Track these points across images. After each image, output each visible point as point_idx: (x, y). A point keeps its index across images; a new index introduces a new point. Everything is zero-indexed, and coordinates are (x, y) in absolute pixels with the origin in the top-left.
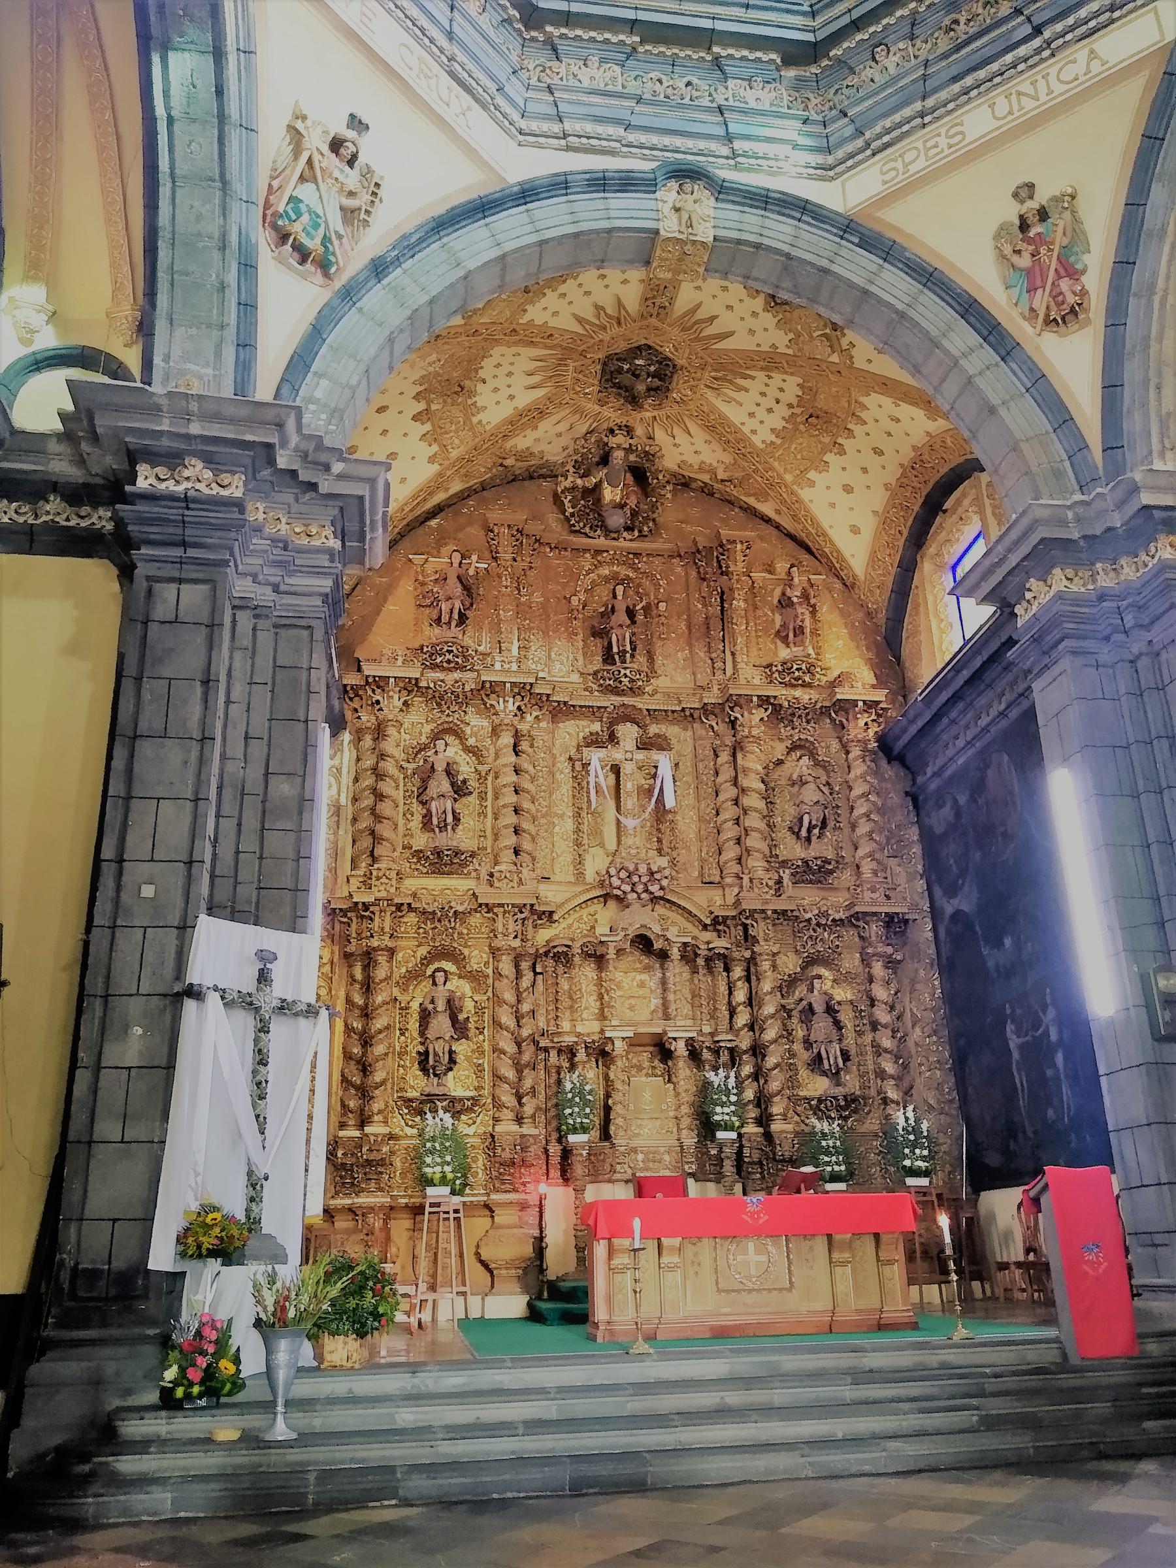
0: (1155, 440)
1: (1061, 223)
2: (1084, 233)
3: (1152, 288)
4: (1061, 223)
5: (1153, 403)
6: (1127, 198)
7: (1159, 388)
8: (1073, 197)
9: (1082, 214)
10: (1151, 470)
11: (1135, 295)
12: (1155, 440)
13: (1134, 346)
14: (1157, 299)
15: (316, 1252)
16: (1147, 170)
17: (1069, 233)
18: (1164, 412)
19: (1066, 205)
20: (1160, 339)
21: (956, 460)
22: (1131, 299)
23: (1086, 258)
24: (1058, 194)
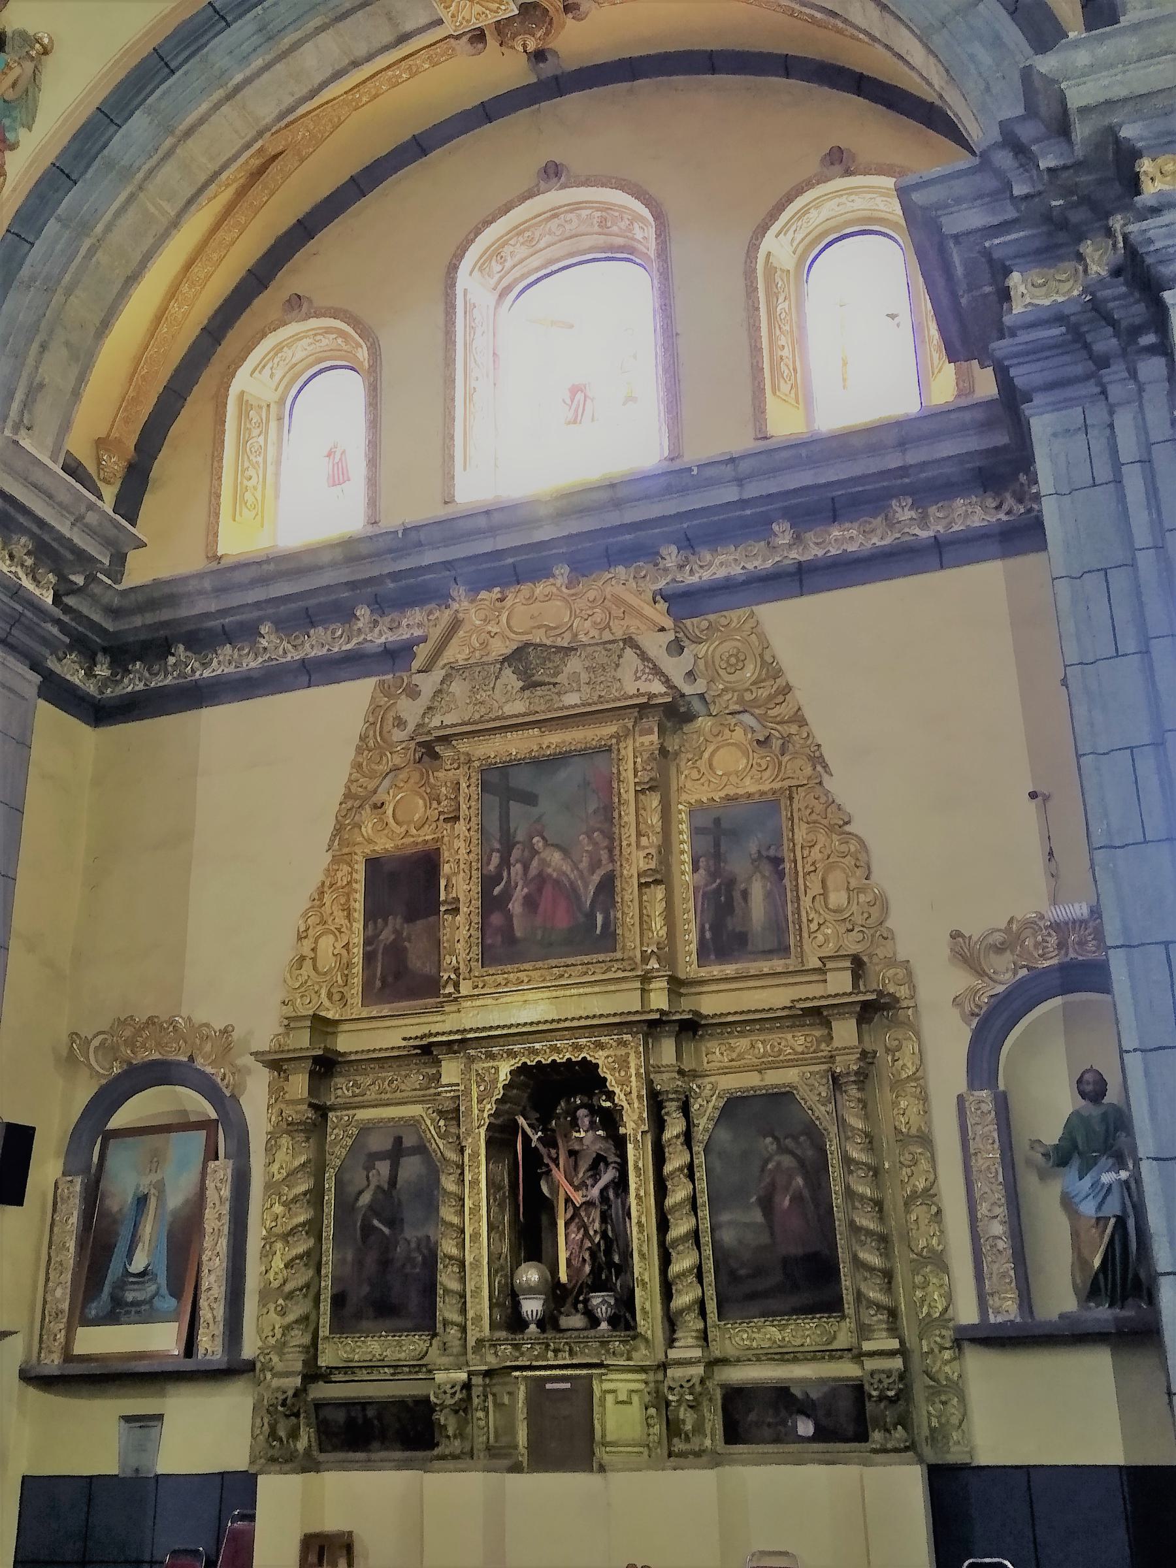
0: (15, 406)
1: (17, 71)
2: (35, 101)
3: (85, 228)
4: (17, 71)
5: (30, 361)
6: (57, 158)
7: (44, 347)
8: (46, 52)
9: (47, 78)
10: (16, 443)
11: (59, 219)
12: (15, 406)
13: (33, 279)
14: (87, 243)
15: (771, 295)
16: (139, 92)
17: (20, 87)
18: (38, 380)
19: (33, 53)
20: (69, 292)
21: (32, 1392)
22: (52, 220)
23: (22, 133)
24: (31, 32)
